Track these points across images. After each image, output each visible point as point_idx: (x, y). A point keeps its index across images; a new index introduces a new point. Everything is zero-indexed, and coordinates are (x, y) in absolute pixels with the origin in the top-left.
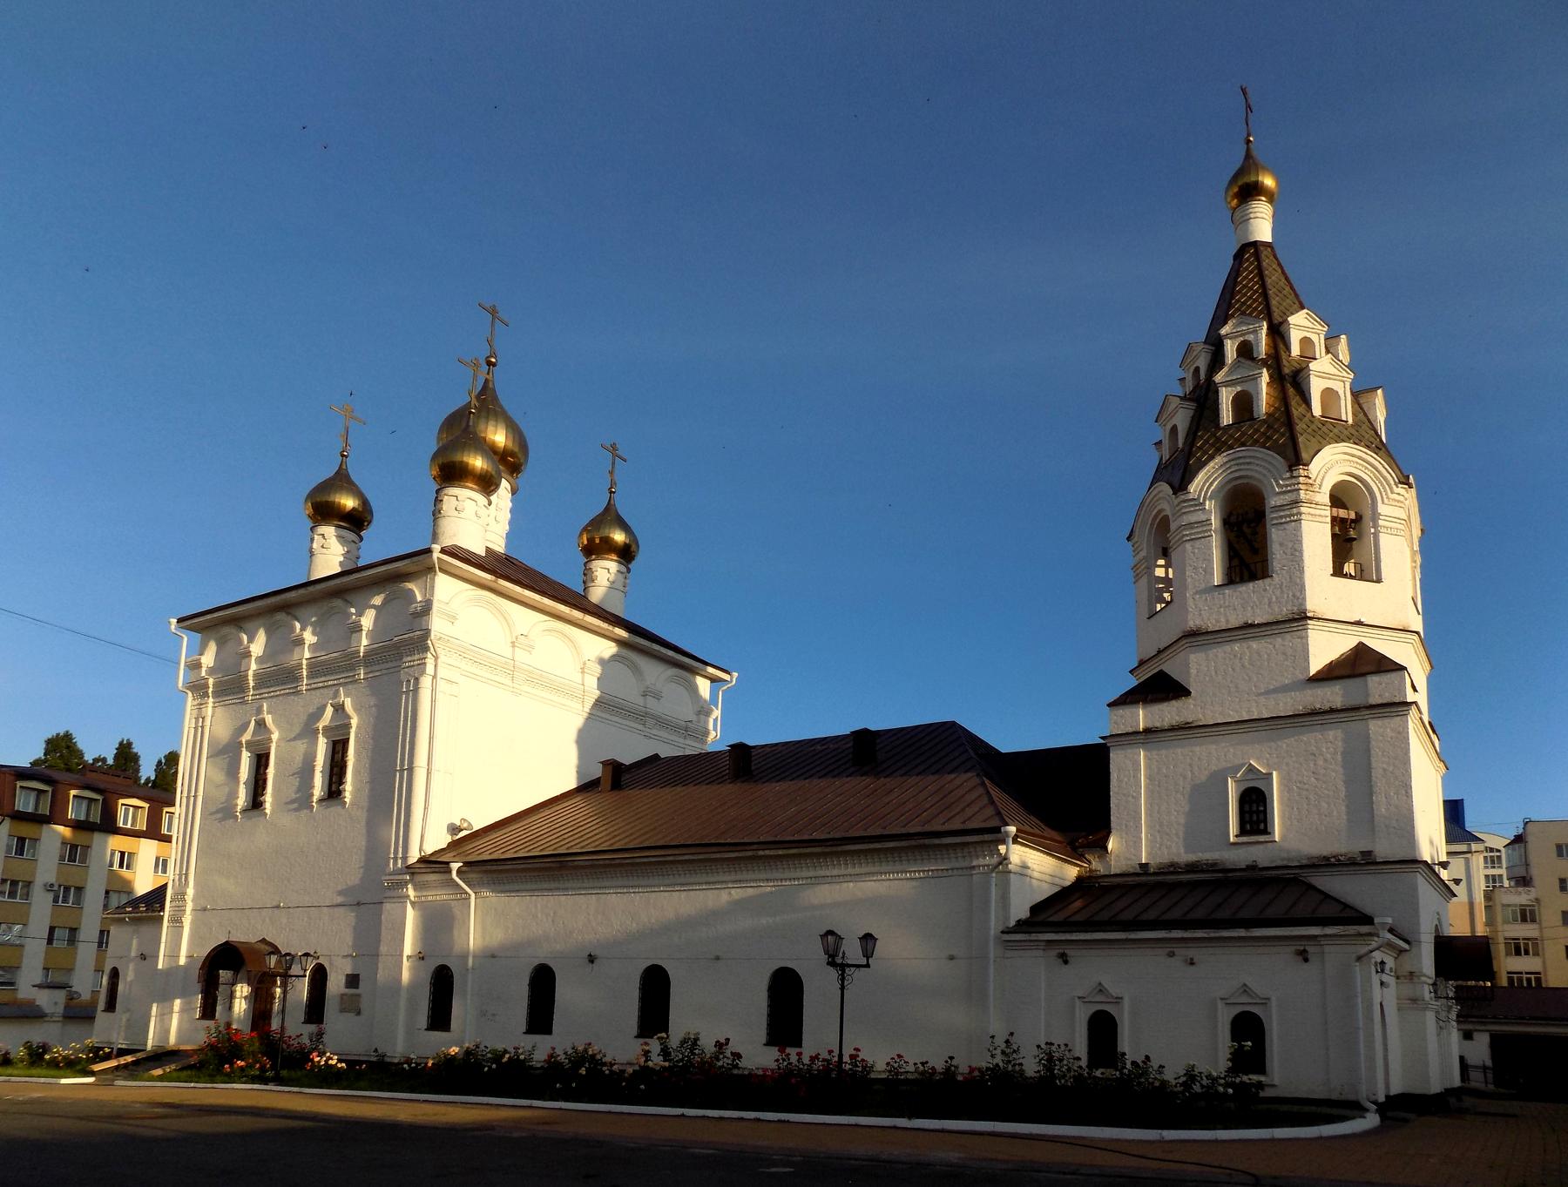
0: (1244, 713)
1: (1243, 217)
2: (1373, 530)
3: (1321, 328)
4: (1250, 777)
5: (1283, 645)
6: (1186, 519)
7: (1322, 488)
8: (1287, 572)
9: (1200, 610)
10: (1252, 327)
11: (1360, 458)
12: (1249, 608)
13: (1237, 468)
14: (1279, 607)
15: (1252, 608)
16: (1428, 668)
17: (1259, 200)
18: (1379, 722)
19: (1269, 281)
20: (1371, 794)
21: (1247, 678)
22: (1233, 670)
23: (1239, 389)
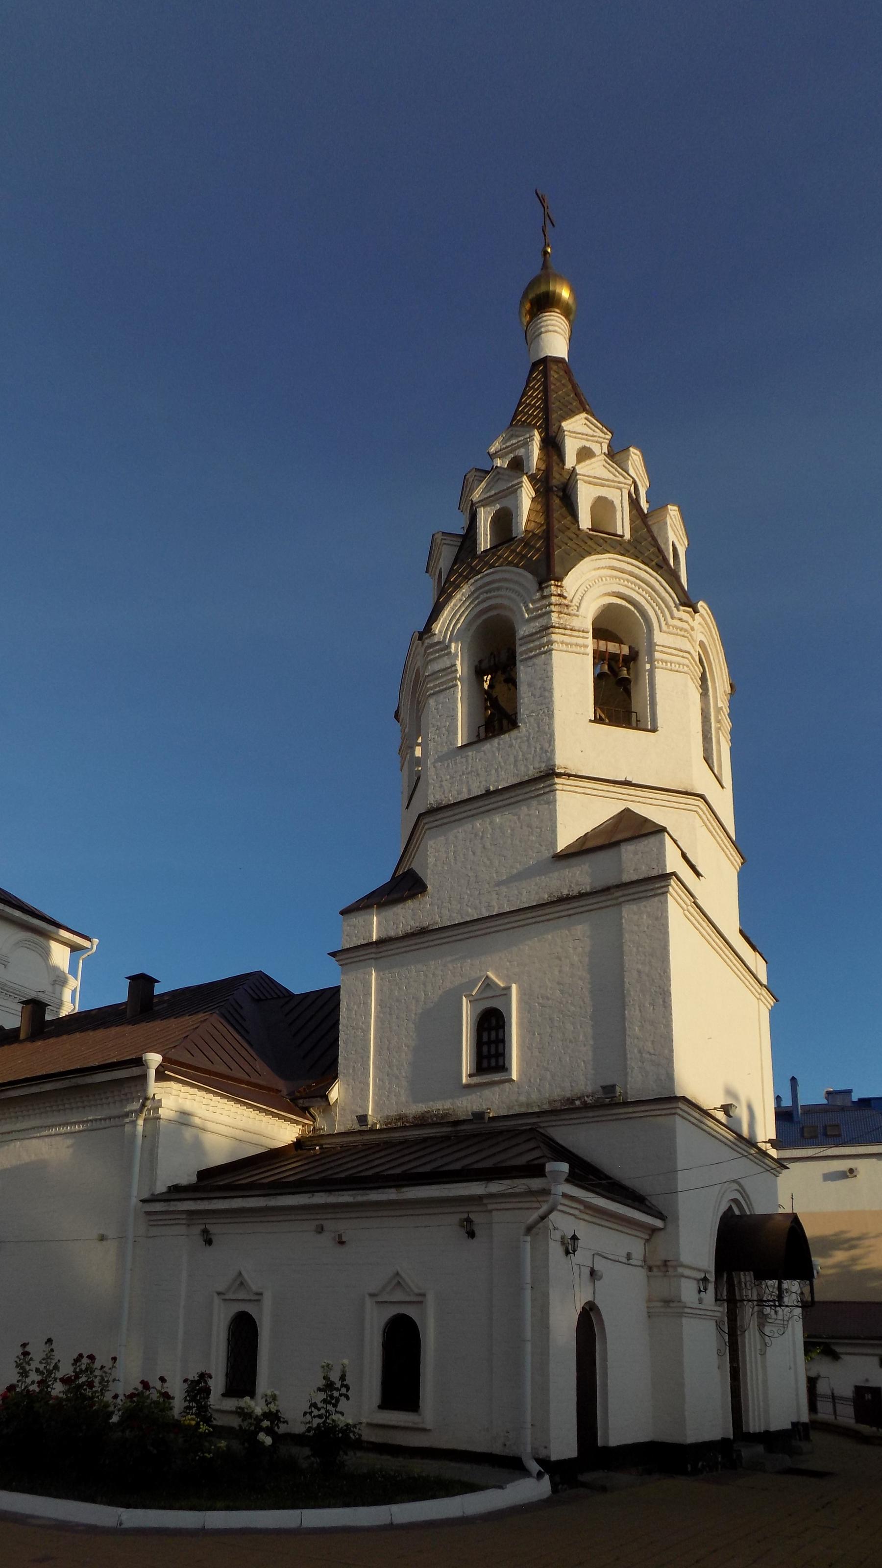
0: (484, 910)
1: (534, 333)
2: (648, 666)
3: (603, 435)
4: (489, 993)
5: (529, 815)
6: (431, 668)
7: (581, 610)
8: (535, 720)
9: (442, 781)
10: (522, 438)
11: (631, 574)
12: (493, 771)
13: (485, 595)
14: (526, 766)
15: (496, 770)
16: (739, 860)
17: (554, 312)
18: (634, 907)
19: (553, 396)
20: (623, 1007)
21: (488, 862)
22: (474, 854)
23: (498, 506)
